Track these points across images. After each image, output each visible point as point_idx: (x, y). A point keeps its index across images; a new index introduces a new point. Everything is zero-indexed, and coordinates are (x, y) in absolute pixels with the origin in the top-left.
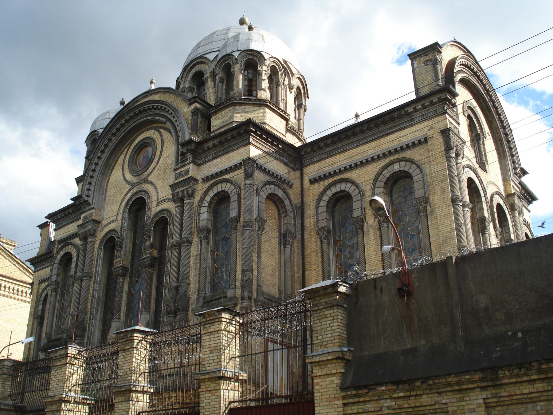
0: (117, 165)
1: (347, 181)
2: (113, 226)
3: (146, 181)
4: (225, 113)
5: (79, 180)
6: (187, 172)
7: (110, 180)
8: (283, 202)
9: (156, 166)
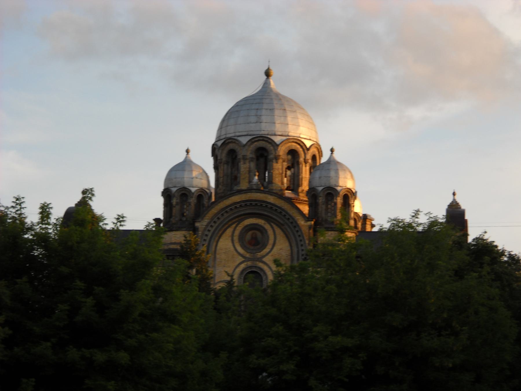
0: (224, 235)
3: (260, 260)
5: (81, 215)
9: (236, 250)
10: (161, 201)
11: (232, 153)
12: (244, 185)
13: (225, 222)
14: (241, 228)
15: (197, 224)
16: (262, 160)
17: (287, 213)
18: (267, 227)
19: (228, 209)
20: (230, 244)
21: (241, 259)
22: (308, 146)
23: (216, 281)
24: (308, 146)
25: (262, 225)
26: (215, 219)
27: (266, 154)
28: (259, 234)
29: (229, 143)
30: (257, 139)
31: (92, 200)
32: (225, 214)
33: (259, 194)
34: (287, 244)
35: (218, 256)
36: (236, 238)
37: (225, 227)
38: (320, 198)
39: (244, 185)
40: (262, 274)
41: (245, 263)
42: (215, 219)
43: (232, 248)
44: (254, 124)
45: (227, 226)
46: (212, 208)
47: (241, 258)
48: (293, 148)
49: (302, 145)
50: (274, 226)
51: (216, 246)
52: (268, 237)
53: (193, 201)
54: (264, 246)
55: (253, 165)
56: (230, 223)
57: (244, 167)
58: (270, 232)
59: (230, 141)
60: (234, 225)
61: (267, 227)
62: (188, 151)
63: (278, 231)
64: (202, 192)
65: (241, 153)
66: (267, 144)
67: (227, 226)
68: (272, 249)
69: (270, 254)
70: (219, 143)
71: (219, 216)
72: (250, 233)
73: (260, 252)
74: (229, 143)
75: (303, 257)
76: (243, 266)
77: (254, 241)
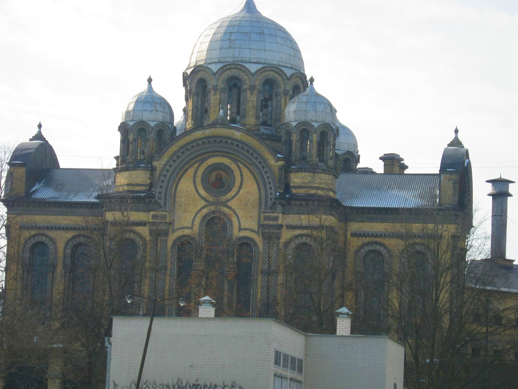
0: (185, 175)
1: (381, 244)
2: (187, 232)
3: (225, 204)
4: (306, 176)
5: (117, 158)
6: (276, 219)
7: (179, 187)
8: (298, 214)
9: (235, 195)
10: (118, 137)
11: (202, 84)
12: (212, 118)
13: (185, 161)
14: (204, 168)
15: (155, 163)
16: (235, 91)
17: (255, 151)
18: (233, 166)
19: (189, 147)
20: (192, 186)
21: (203, 203)
22: (288, 75)
24: (288, 75)
26: (175, 158)
27: (239, 85)
28: (224, 174)
29: (198, 71)
30: (228, 67)
31: (407, 167)
33: (224, 130)
35: (177, 199)
36: (198, 180)
37: (186, 167)
38: (294, 135)
39: (212, 118)
42: (175, 158)
44: (226, 50)
45: (188, 165)
46: (172, 144)
48: (271, 77)
49: (280, 73)
50: (241, 166)
51: (176, 187)
53: (152, 136)
54: (229, 189)
55: (224, 96)
56: (192, 162)
57: (214, 98)
58: (237, 173)
59: (200, 68)
60: (196, 165)
61: (233, 166)
62: (456, 131)
63: (245, 171)
64: (163, 126)
65: (211, 82)
66: (241, 72)
67: (188, 165)
68: (238, 192)
69: (236, 198)
70: (189, 72)
71: (179, 154)
73: (225, 195)
74: (198, 71)
75: (272, 202)
76: (205, 211)
77: (218, 183)
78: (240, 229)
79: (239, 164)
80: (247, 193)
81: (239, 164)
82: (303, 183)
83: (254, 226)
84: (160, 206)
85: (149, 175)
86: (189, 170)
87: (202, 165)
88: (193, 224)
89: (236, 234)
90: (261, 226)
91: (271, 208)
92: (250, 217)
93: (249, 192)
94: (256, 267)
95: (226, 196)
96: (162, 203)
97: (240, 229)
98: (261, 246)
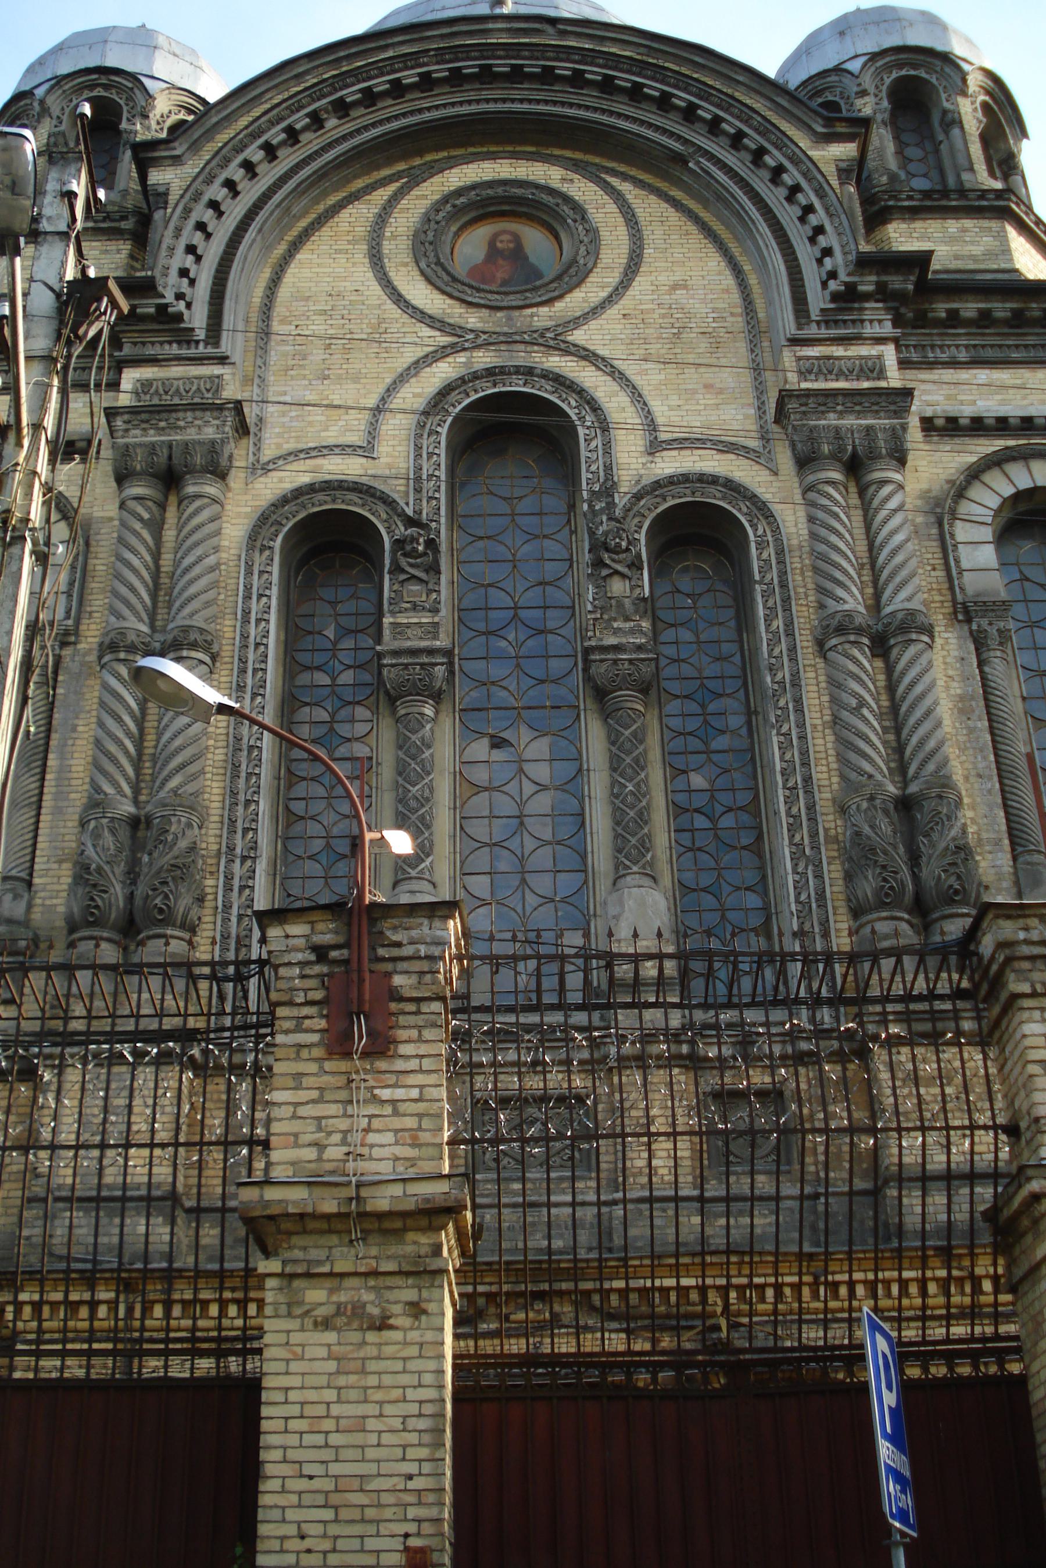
0: (326, 231)
3: (556, 340)
20: (364, 276)
23: (268, 453)
25: (556, 184)
28: (534, 240)
32: (332, 123)
34: (715, 262)
40: (570, 407)
41: (462, 358)
43: (374, 290)
47: (426, 332)
51: (275, 281)
52: (594, 234)
58: (603, 213)
60: (383, 194)
61: (582, 190)
63: (648, 207)
72: (482, 233)
78: (655, 446)
79: (609, 179)
80: (675, 287)
81: (609, 179)
82: (957, 257)
83: (737, 418)
84: (185, 337)
85: (124, 254)
86: (344, 214)
87: (415, 192)
88: (373, 432)
89: (633, 463)
90: (785, 408)
91: (828, 319)
92: (706, 386)
93: (685, 287)
94: (779, 623)
95: (559, 305)
96: (198, 319)
97: (655, 446)
98: (793, 521)
